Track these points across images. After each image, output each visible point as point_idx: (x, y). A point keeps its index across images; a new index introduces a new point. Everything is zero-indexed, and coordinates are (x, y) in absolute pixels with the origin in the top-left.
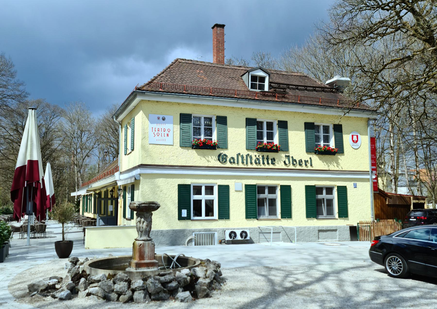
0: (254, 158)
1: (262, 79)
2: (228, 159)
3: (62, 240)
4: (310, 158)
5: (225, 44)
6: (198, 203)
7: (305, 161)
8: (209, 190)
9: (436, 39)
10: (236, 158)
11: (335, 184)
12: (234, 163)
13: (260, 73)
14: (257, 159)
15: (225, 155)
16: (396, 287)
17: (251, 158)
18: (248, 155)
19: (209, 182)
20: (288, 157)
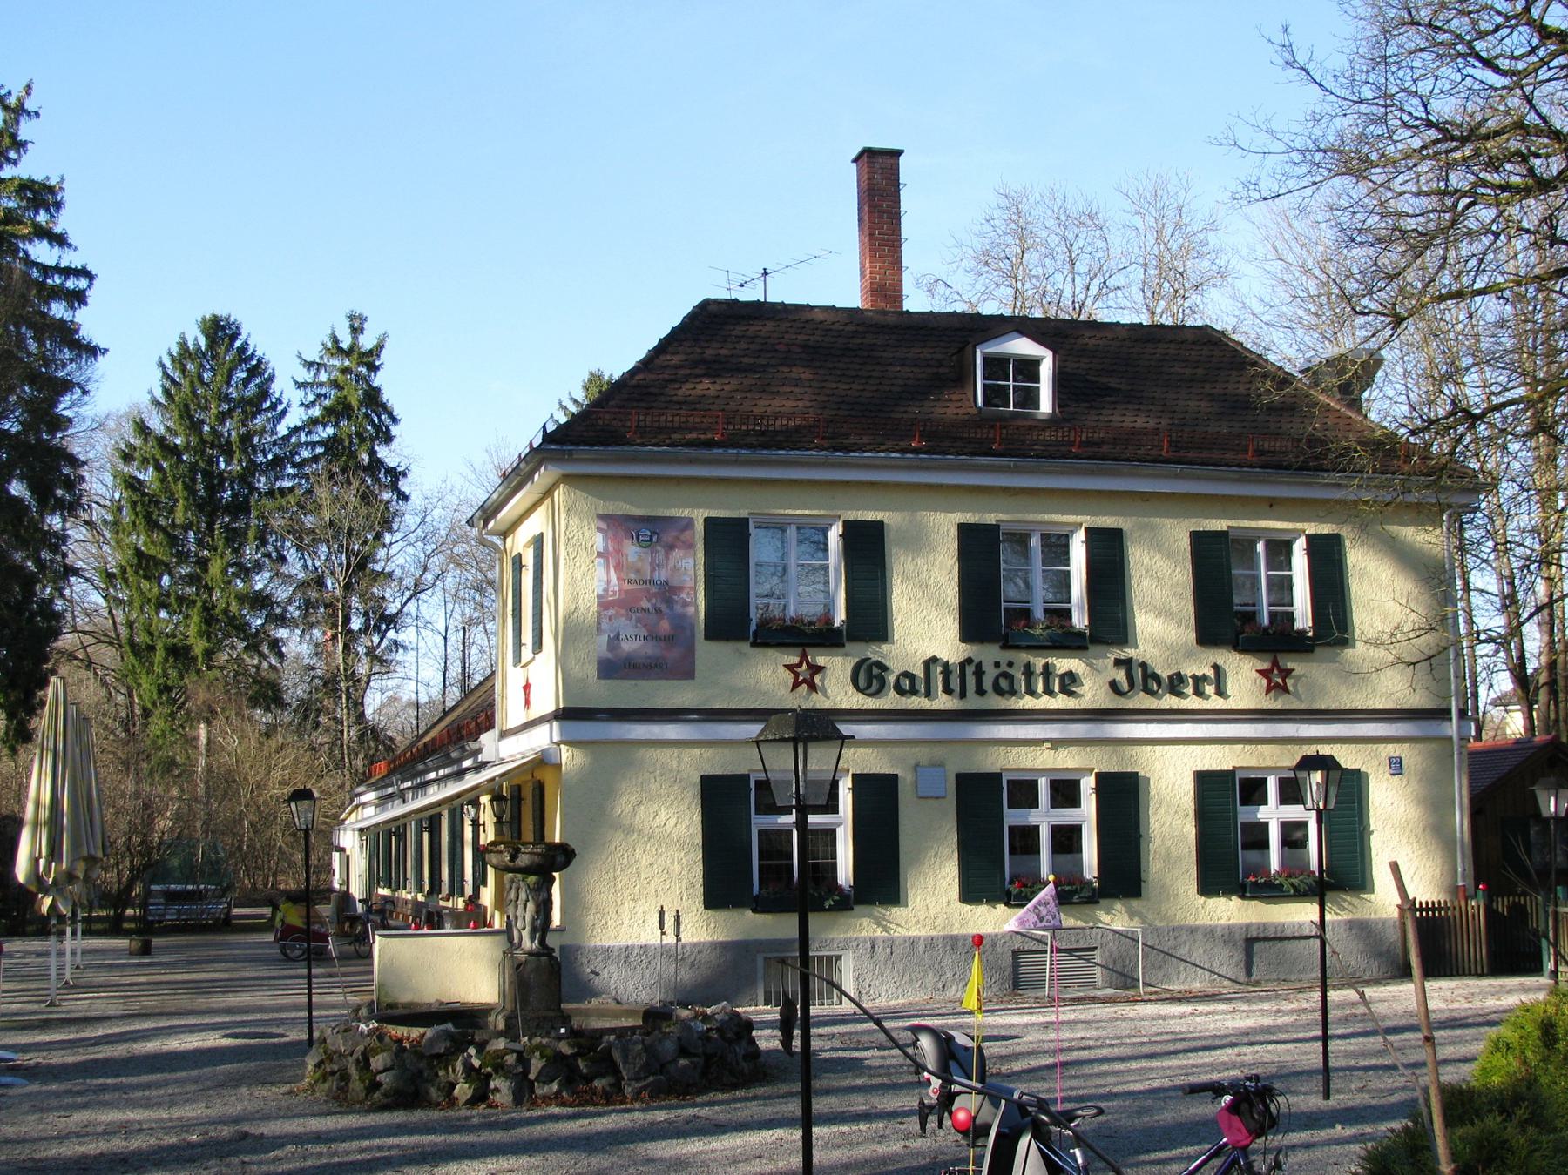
0: (990, 675)
1: (1029, 368)
2: (892, 679)
3: (814, 920)
4: (1216, 667)
5: (617, 365)
6: (1026, 839)
7: (1194, 677)
8: (1065, 792)
9: (4, 531)
10: (920, 673)
11: (1038, 764)
12: (914, 692)
13: (1023, 346)
14: (1005, 675)
15: (879, 665)
16: (580, 1012)
17: (979, 673)
18: (969, 661)
19: (1066, 760)
20: (1125, 664)
